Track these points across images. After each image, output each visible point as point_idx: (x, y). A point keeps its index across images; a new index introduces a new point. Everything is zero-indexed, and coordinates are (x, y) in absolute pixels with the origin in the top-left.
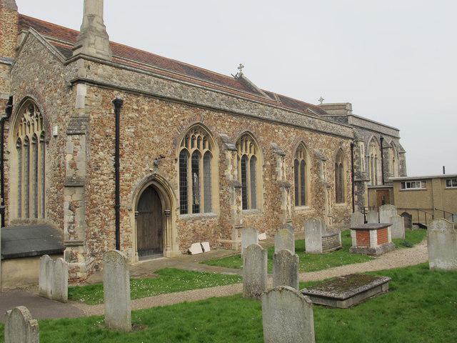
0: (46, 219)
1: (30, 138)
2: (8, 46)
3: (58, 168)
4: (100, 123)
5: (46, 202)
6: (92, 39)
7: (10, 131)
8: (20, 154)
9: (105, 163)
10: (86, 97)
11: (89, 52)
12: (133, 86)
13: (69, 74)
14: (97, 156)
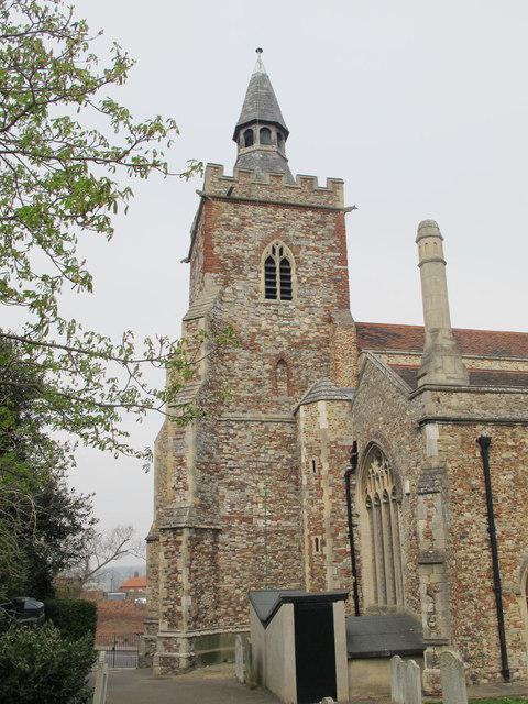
0: (403, 606)
1: (390, 493)
4: (462, 473)
5: (405, 582)
6: (438, 361)
7: (358, 487)
8: (372, 517)
9: (474, 527)
10: (438, 441)
12: (504, 414)
13: (415, 412)
14: (462, 519)
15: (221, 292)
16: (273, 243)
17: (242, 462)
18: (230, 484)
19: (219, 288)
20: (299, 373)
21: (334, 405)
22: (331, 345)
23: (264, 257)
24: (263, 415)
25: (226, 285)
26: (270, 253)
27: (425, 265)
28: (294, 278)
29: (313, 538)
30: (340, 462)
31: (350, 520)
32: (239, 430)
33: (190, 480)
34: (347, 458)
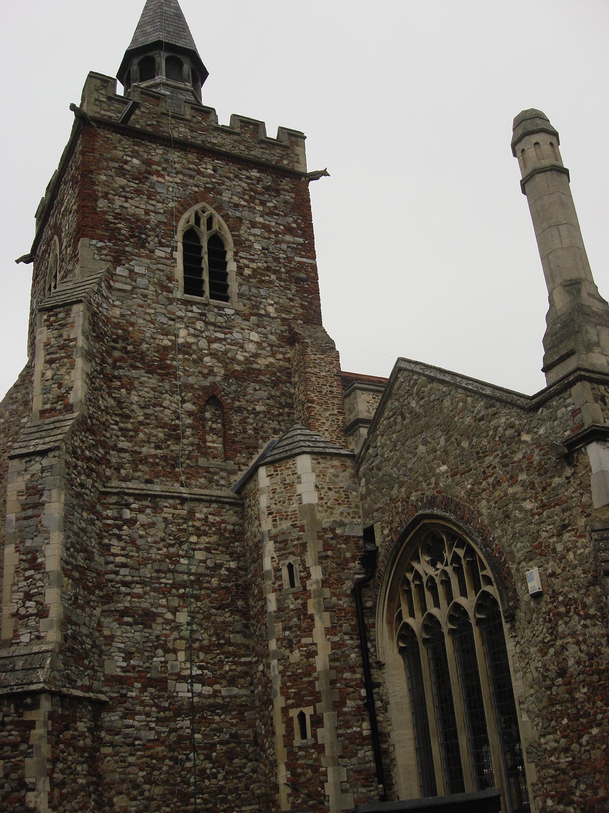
2: (328, 424)
3: (560, 681)
11: (592, 365)
15: (108, 270)
16: (197, 207)
17: (147, 572)
18: (124, 613)
19: (105, 266)
20: (244, 421)
21: (325, 464)
22: (296, 379)
23: (182, 226)
24: (183, 490)
25: (117, 262)
26: (192, 221)
27: (539, 178)
28: (232, 267)
29: (294, 713)
30: (343, 564)
31: (367, 674)
32: (141, 511)
33: (52, 597)
34: (354, 559)
